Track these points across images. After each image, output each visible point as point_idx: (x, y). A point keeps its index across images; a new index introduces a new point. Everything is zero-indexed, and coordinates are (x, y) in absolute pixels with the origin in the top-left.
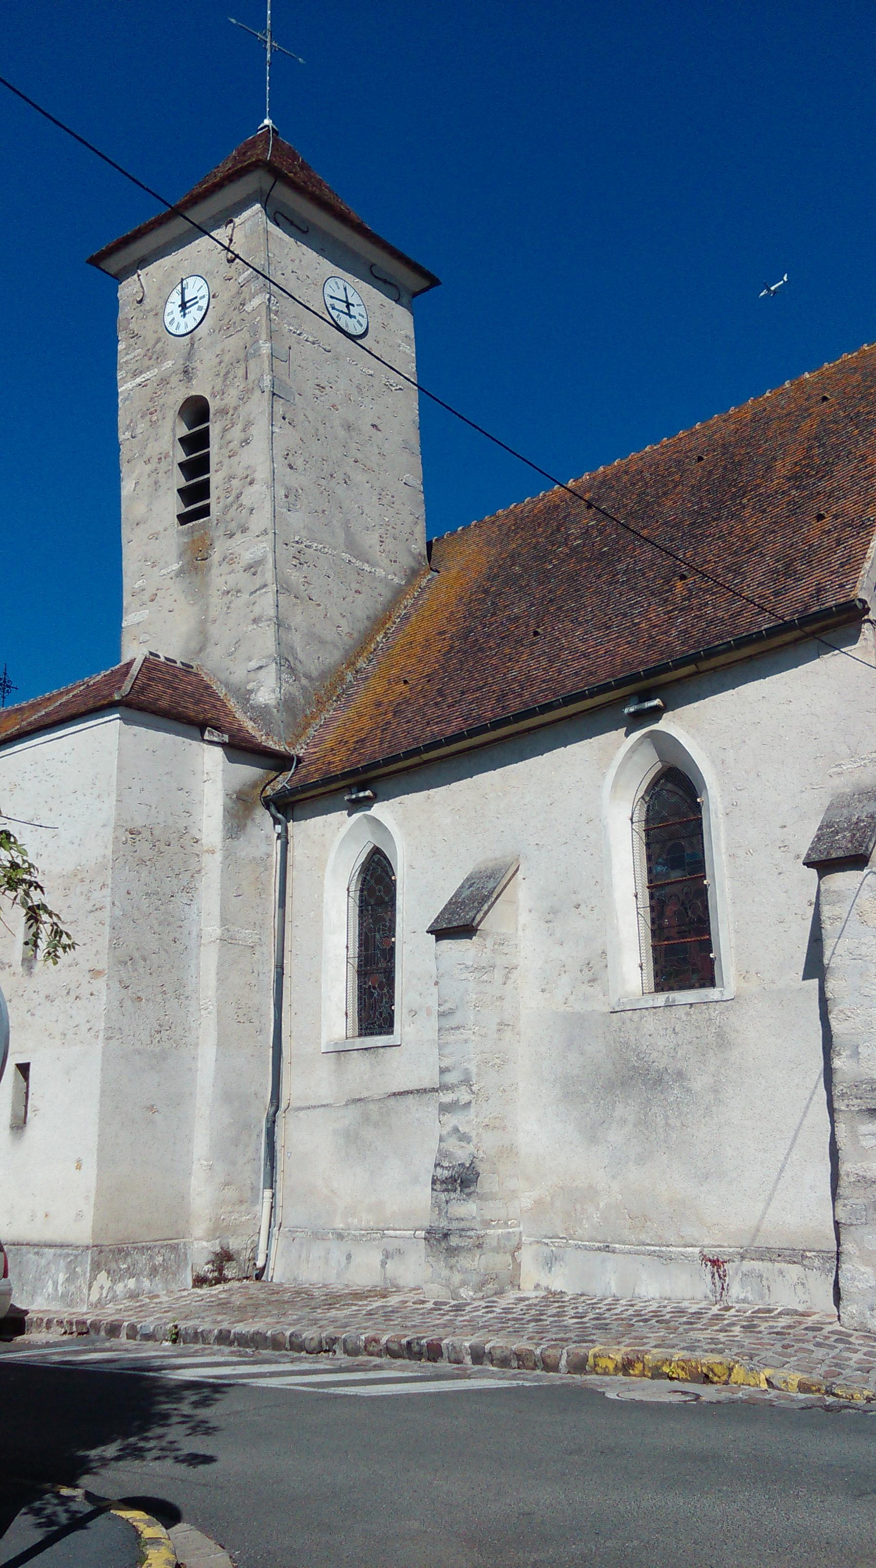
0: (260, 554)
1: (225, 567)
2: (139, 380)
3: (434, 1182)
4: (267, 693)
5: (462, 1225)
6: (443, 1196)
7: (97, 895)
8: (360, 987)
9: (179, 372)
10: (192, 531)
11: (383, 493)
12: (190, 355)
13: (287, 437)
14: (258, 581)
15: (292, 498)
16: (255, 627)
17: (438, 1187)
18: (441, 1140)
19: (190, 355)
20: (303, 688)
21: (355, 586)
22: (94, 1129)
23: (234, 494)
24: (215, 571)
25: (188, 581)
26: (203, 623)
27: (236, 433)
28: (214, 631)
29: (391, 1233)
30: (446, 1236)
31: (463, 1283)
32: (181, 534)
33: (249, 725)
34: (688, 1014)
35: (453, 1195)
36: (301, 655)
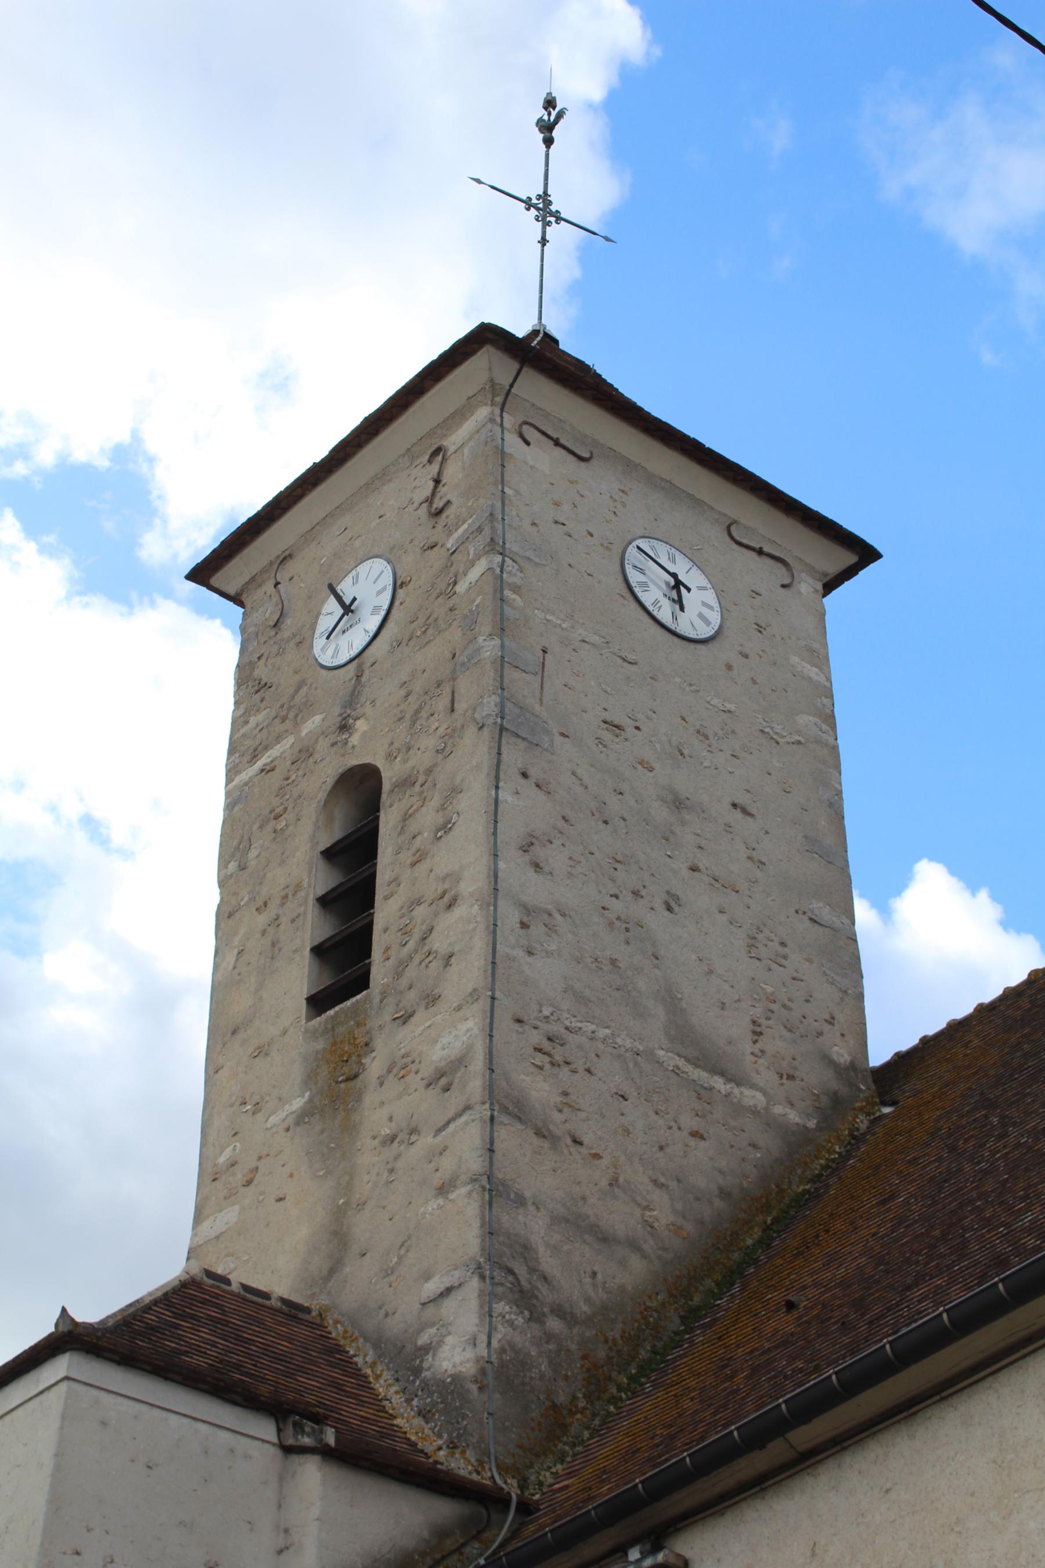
1: (393, 1087)
2: (259, 764)
4: (455, 1356)
9: (333, 729)
10: (331, 1029)
11: (760, 936)
12: (352, 700)
14: (455, 1100)
15: (537, 930)
16: (441, 1201)
19: (352, 700)
20: (549, 1337)
21: (689, 1122)
23: (416, 935)
24: (370, 1098)
25: (318, 1128)
27: (428, 818)
28: (362, 1227)
33: (408, 1422)
36: (548, 1263)
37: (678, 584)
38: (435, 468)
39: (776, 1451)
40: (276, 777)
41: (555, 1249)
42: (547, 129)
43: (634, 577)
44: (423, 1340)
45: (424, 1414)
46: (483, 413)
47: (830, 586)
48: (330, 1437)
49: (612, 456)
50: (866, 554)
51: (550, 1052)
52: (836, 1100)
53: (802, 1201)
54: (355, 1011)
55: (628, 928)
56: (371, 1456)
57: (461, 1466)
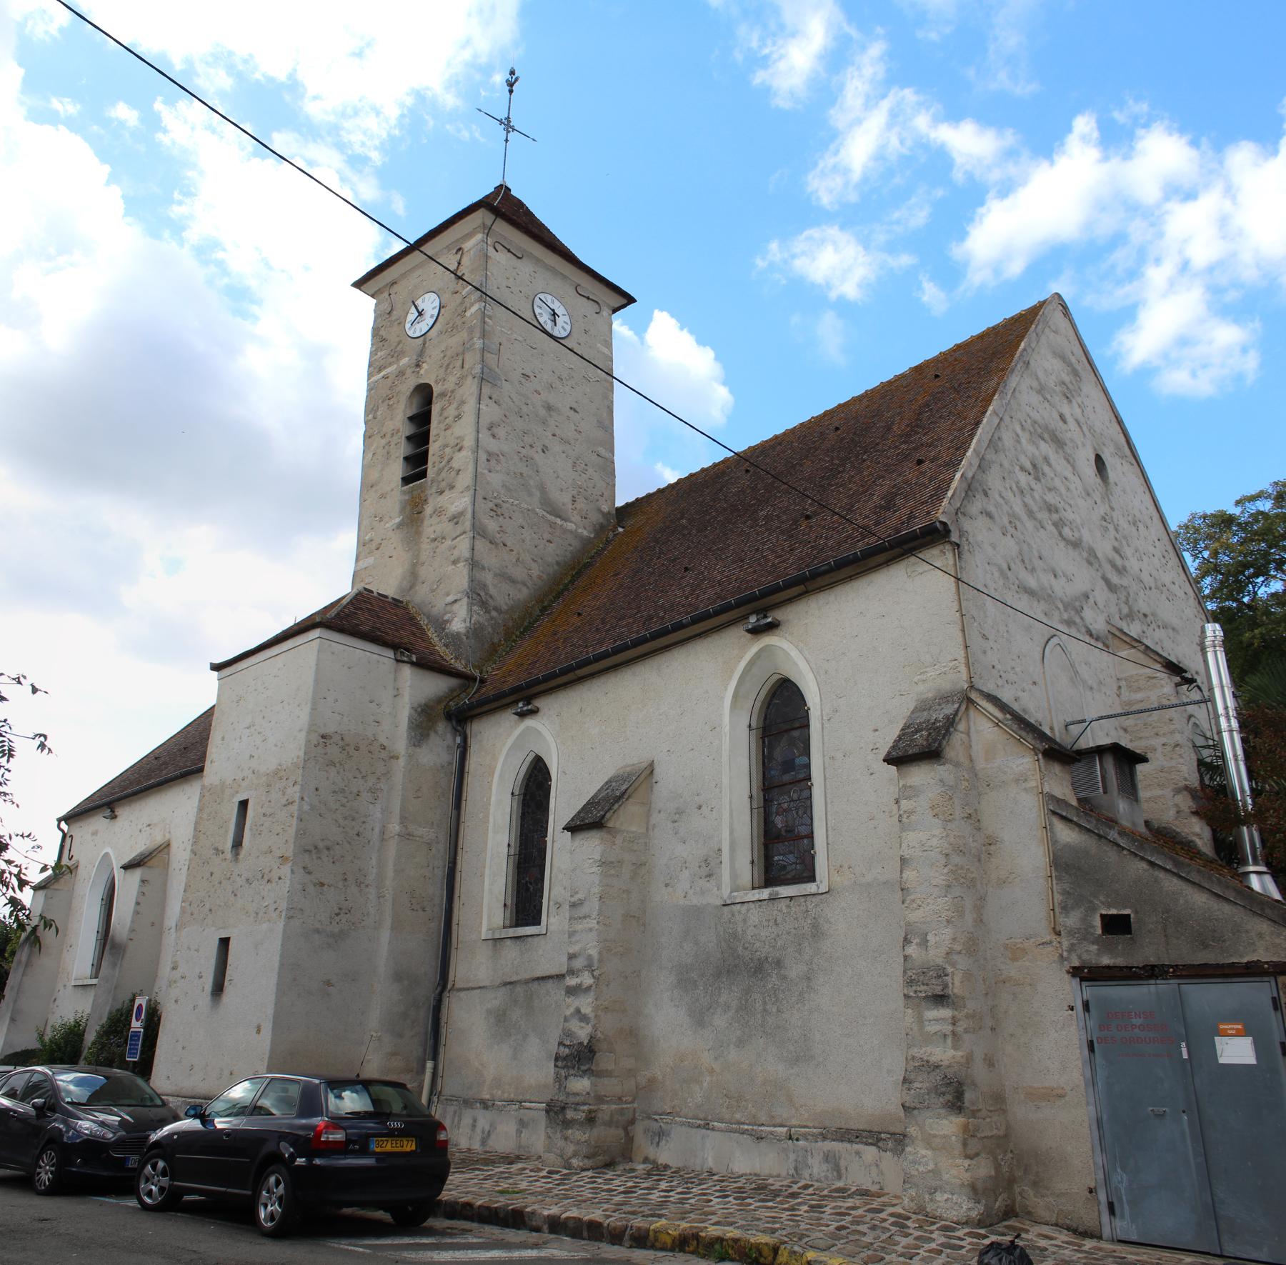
0: (460, 508)
1: (435, 519)
3: (556, 1059)
4: (458, 625)
5: (578, 1099)
6: (563, 1072)
7: (289, 791)
8: (518, 882)
12: (421, 353)
13: (490, 412)
14: (459, 529)
15: (493, 462)
17: (560, 1064)
18: (566, 1020)
19: (421, 353)
20: (492, 618)
21: (547, 536)
22: (272, 998)
24: (426, 523)
26: (414, 566)
27: (451, 411)
28: (423, 572)
29: (527, 1104)
30: (563, 1109)
31: (575, 1155)
32: (404, 493)
33: (440, 648)
34: (788, 907)
35: (571, 1072)
36: (492, 591)
37: (554, 314)
38: (458, 257)
39: (570, 676)
40: (389, 381)
41: (495, 586)
42: (511, 85)
43: (537, 311)
44: (446, 618)
45: (446, 645)
46: (479, 236)
47: (615, 311)
48: (414, 659)
49: (531, 256)
50: (631, 300)
51: (496, 511)
52: (602, 526)
53: (587, 566)
54: (421, 486)
55: (527, 460)
56: (428, 664)
57: (459, 666)
